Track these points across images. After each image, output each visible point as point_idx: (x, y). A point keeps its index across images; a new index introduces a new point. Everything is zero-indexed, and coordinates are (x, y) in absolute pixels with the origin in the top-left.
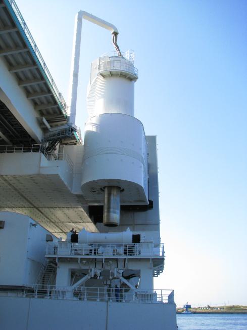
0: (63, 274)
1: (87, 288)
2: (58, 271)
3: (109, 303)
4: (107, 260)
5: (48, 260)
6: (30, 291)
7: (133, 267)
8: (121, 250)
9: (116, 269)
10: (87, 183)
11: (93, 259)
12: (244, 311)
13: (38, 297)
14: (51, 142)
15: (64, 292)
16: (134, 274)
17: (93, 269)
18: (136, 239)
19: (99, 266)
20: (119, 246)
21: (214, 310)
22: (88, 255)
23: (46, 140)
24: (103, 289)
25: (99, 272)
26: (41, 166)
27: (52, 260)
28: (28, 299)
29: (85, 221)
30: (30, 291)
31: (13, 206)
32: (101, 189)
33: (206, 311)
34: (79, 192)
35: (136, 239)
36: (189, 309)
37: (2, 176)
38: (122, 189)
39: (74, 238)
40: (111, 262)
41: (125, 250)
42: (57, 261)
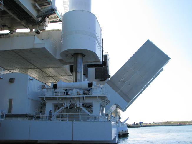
0: (49, 106)
2: (46, 105)
4: (73, 98)
5: (40, 99)
6: (31, 117)
7: (87, 101)
8: (82, 92)
9: (78, 103)
10: (63, 52)
12: (173, 124)
14: (42, 17)
16: (91, 106)
17: (65, 104)
18: (90, 85)
19: (69, 102)
20: (80, 89)
21: (156, 124)
22: (64, 95)
23: (38, 17)
24: (78, 114)
25: (69, 105)
27: (42, 99)
28: (29, 121)
29: (69, 75)
30: (31, 117)
31: (25, 68)
32: (72, 55)
33: (152, 125)
35: (90, 85)
36: (142, 124)
38: (84, 55)
40: (75, 99)
41: (84, 92)
42: (45, 99)
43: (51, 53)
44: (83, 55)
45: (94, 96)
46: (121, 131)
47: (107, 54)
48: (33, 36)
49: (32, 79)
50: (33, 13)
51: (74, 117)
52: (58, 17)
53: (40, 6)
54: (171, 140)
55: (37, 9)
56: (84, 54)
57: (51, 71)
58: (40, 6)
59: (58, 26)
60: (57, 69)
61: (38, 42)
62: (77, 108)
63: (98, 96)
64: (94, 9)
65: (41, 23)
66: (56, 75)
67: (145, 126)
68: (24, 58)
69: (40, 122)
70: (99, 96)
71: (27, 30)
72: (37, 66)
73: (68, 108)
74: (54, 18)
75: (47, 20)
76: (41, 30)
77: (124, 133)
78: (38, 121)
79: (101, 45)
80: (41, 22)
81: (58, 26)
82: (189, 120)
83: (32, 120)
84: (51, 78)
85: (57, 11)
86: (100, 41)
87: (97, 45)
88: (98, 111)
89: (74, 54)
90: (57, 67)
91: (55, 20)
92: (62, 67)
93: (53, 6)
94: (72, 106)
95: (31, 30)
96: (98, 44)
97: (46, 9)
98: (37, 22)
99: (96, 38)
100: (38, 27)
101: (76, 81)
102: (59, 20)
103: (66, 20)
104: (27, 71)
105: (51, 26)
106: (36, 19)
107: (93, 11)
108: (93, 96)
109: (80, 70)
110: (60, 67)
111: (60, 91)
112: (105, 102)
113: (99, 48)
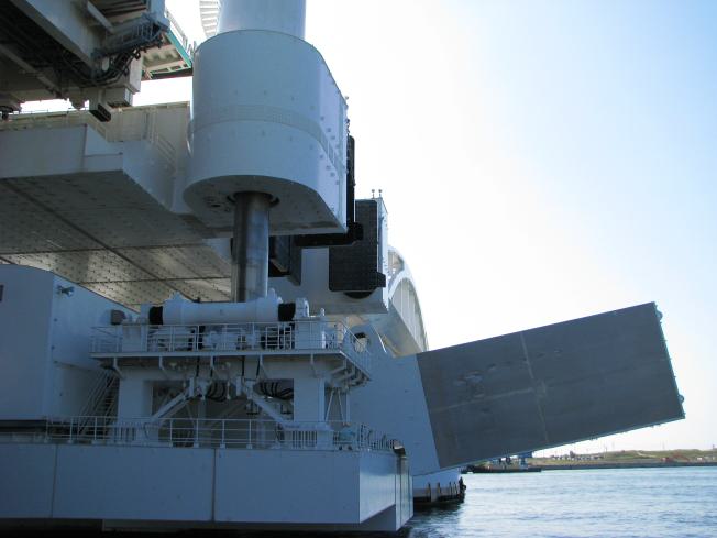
0: (132, 395)
1: (226, 423)
3: (218, 451)
4: (220, 361)
5: (100, 363)
6: (60, 431)
7: (274, 373)
8: (253, 338)
9: (239, 380)
11: (193, 358)
12: (642, 461)
13: (227, 446)
14: (114, 57)
15: (314, 434)
18: (286, 312)
19: (204, 374)
20: (248, 328)
21: (582, 462)
22: (181, 350)
23: (101, 54)
25: (204, 386)
26: (87, 153)
28: (53, 447)
30: (60, 431)
32: (228, 198)
33: (565, 464)
34: (186, 210)
35: (286, 312)
37: (5, 179)
38: (274, 199)
39: (156, 316)
40: (229, 364)
41: (263, 338)
42: (115, 366)
43: (149, 191)
44: (270, 200)
45: (298, 356)
46: (434, 486)
47: (377, 196)
48: (78, 126)
49: (71, 289)
50: (81, 40)
51: (245, 435)
52: (180, 58)
53: (106, 12)
54: (520, 507)
55: (96, 27)
56: (276, 194)
57: (166, 261)
58: (106, 15)
59: (179, 91)
60: (182, 251)
61: (99, 151)
62: (235, 398)
63: (312, 353)
64: (317, 30)
65: (110, 77)
66: (181, 276)
67: (538, 469)
68: (50, 210)
69: (94, 450)
70: (315, 356)
71: (61, 106)
72: (106, 243)
73: (203, 398)
74: (164, 62)
75: (136, 66)
76: (113, 106)
77: (444, 494)
78: (85, 447)
79: (345, 163)
80: (110, 74)
81: (179, 91)
82: (704, 446)
83: (65, 442)
84: (162, 285)
85: (172, 28)
86: (338, 146)
87: (326, 161)
88: (310, 404)
89: (236, 194)
90: (180, 243)
91: (169, 66)
92: (198, 245)
93: (155, 13)
94: (217, 396)
95: (78, 104)
96: (330, 157)
97: (130, 24)
98: (93, 75)
99: (315, 133)
100: (104, 94)
101: (241, 298)
102: (183, 68)
103: (206, 65)
104: (88, 259)
105: (151, 93)
106: (89, 63)
107: (311, 35)
108: (297, 353)
109: (260, 256)
110: (191, 245)
111: (174, 333)
112: (343, 377)
113: (332, 175)
